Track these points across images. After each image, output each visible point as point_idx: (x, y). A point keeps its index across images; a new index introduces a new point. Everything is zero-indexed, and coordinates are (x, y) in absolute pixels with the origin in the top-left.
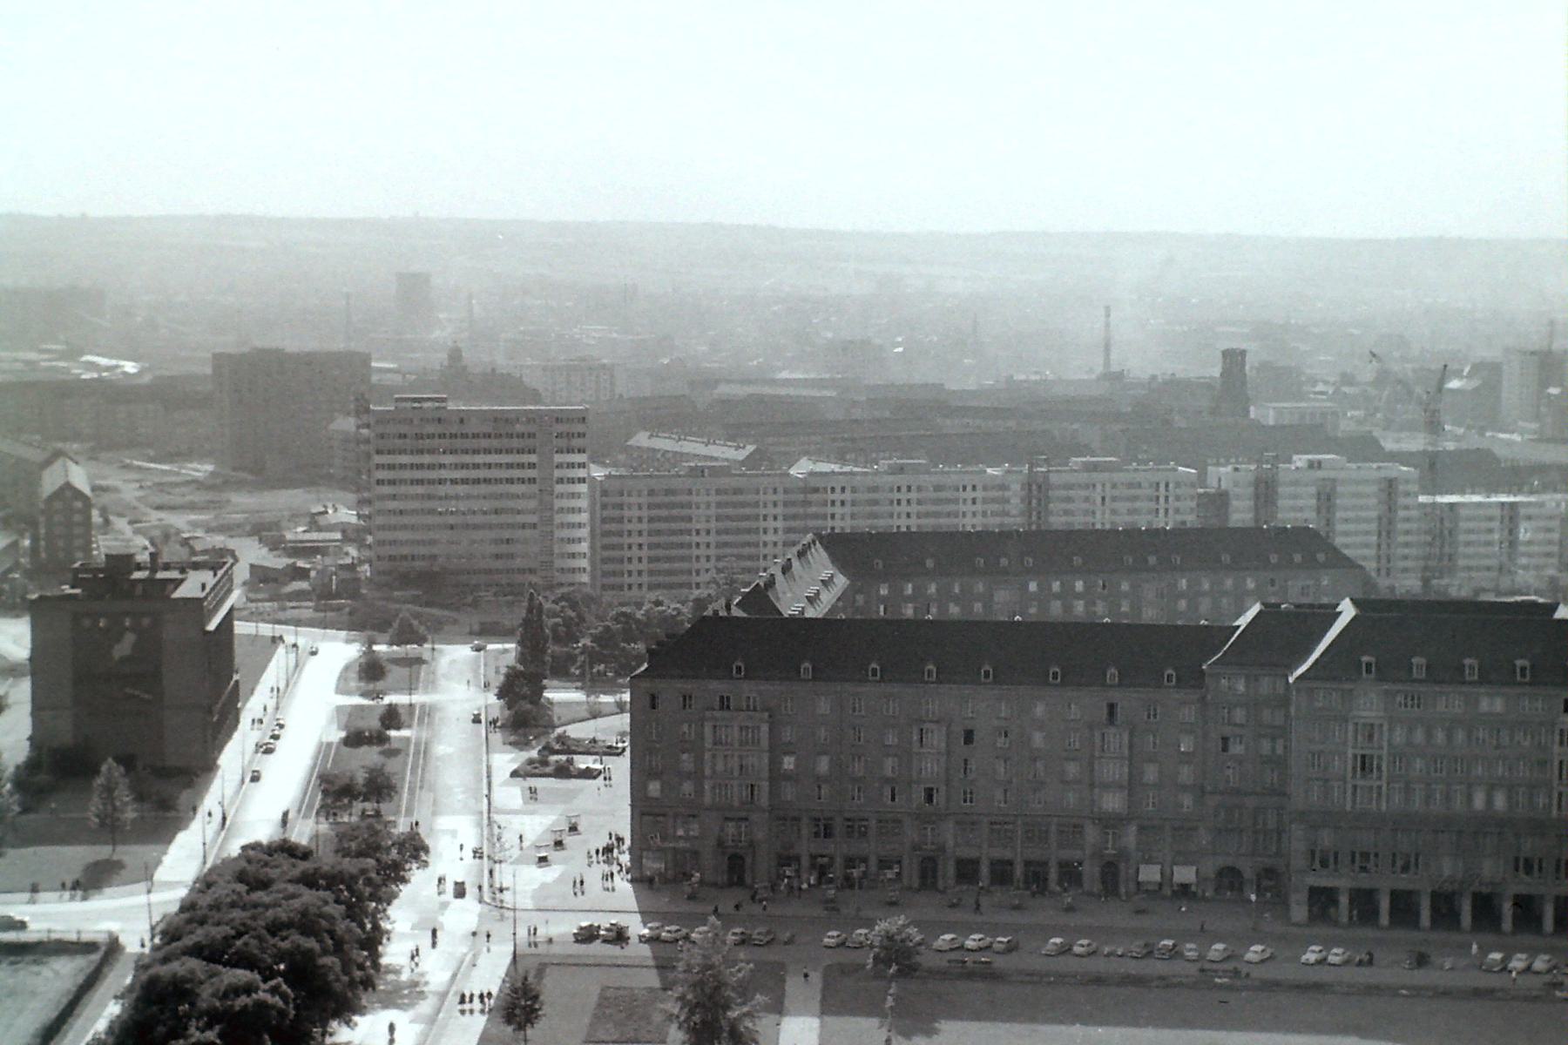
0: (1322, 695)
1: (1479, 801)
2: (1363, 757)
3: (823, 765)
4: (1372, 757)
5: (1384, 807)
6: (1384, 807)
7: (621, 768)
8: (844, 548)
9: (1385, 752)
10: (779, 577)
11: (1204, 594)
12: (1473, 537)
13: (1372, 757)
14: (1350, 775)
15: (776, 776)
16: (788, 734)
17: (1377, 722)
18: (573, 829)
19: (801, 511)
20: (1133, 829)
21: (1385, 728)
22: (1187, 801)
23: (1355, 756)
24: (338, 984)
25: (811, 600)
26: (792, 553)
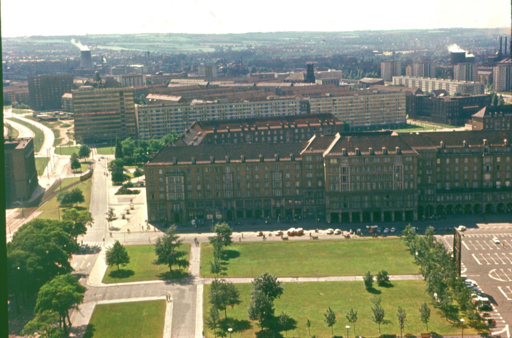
0: (103, 228)
1: (374, 187)
2: (344, 177)
3: (199, 187)
4: (346, 176)
5: (350, 190)
6: (350, 190)
7: (143, 191)
8: (204, 125)
9: (349, 175)
10: (186, 135)
11: (235, 138)
12: (128, 98)
13: (346, 176)
14: (340, 181)
15: (186, 191)
16: (188, 179)
17: (347, 167)
18: (132, 209)
19: (347, 115)
20: (284, 200)
21: (349, 168)
22: (298, 191)
23: (341, 176)
24: (353, 160)
25: (195, 140)
26: (189, 127)
